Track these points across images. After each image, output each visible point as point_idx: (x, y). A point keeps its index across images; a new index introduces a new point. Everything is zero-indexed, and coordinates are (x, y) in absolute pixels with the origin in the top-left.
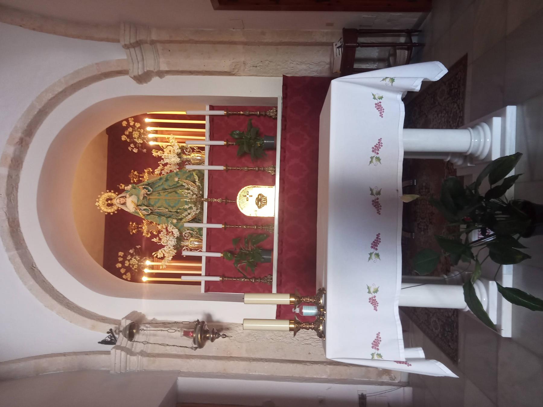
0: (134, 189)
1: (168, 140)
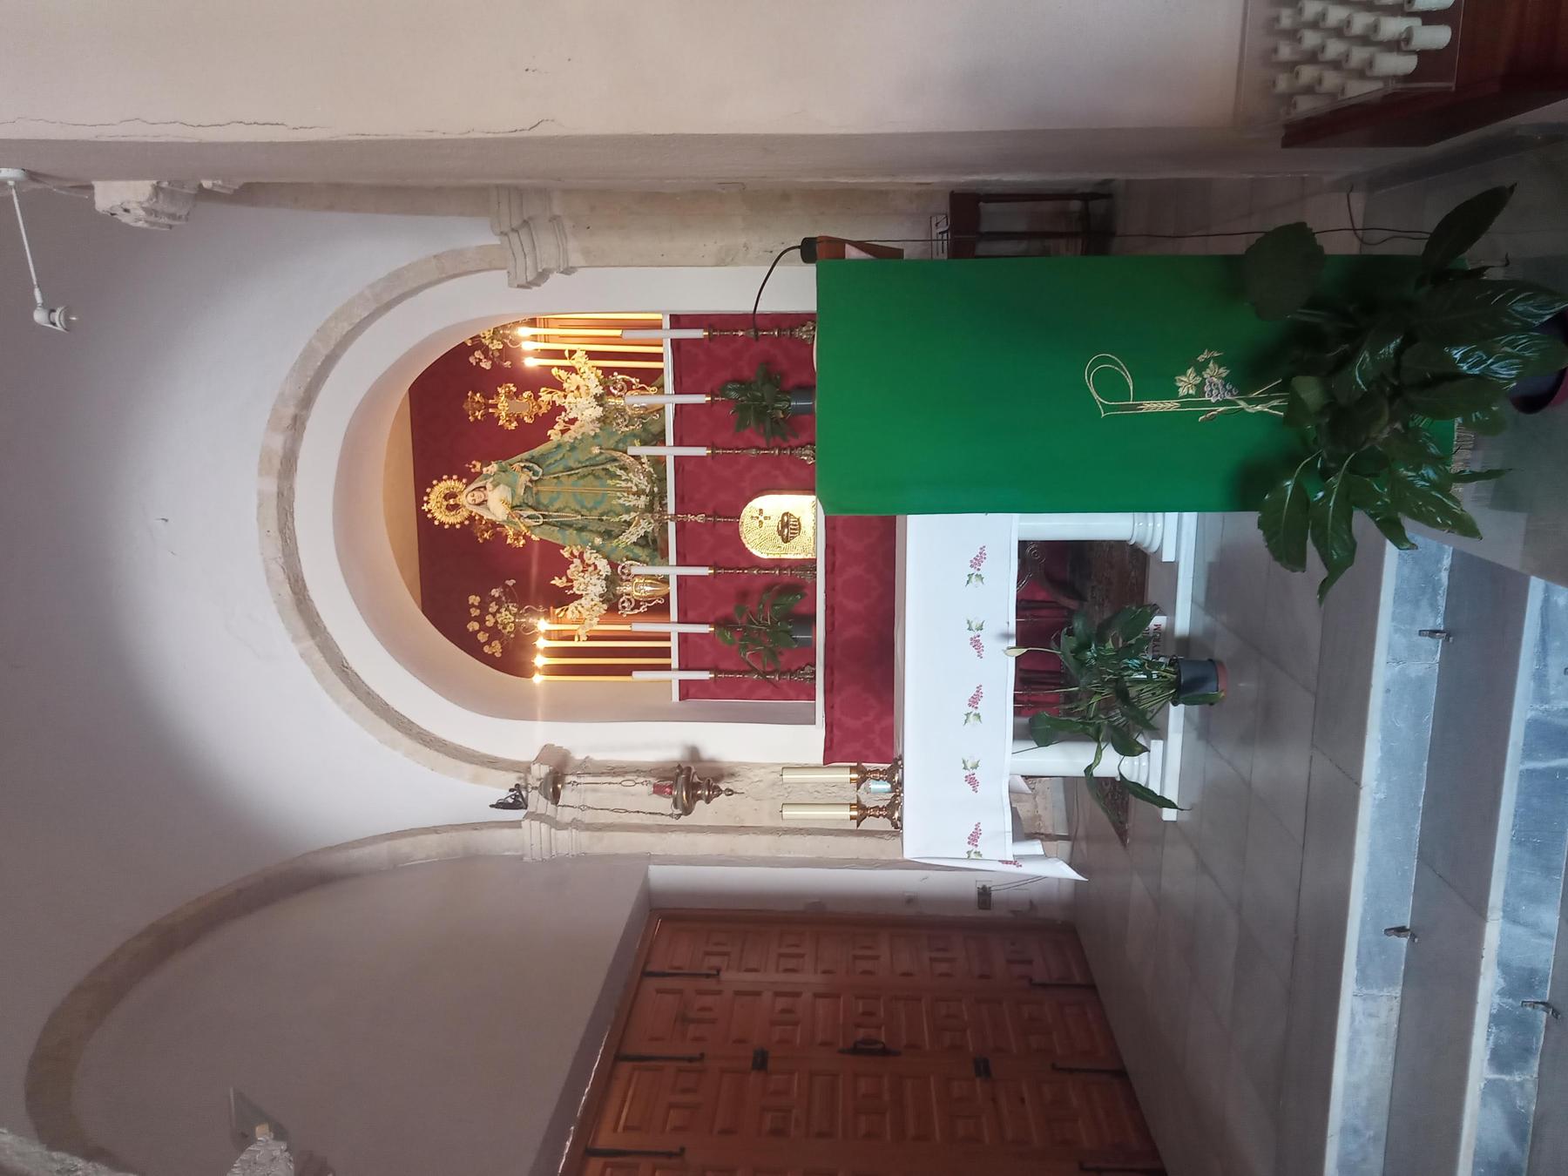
0: (504, 472)
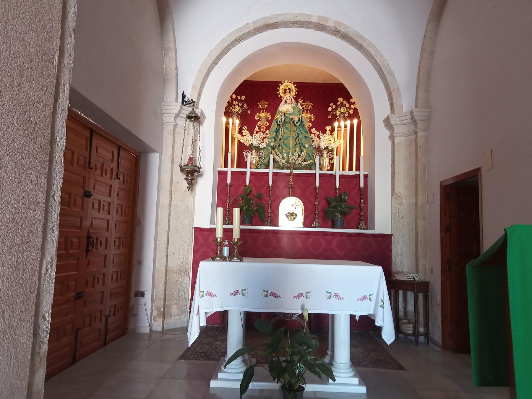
0: (299, 111)
1: (339, 138)
